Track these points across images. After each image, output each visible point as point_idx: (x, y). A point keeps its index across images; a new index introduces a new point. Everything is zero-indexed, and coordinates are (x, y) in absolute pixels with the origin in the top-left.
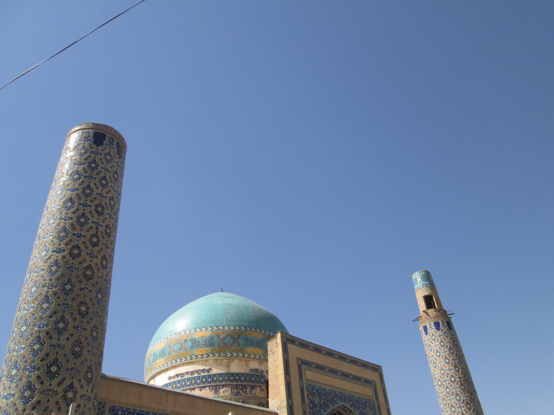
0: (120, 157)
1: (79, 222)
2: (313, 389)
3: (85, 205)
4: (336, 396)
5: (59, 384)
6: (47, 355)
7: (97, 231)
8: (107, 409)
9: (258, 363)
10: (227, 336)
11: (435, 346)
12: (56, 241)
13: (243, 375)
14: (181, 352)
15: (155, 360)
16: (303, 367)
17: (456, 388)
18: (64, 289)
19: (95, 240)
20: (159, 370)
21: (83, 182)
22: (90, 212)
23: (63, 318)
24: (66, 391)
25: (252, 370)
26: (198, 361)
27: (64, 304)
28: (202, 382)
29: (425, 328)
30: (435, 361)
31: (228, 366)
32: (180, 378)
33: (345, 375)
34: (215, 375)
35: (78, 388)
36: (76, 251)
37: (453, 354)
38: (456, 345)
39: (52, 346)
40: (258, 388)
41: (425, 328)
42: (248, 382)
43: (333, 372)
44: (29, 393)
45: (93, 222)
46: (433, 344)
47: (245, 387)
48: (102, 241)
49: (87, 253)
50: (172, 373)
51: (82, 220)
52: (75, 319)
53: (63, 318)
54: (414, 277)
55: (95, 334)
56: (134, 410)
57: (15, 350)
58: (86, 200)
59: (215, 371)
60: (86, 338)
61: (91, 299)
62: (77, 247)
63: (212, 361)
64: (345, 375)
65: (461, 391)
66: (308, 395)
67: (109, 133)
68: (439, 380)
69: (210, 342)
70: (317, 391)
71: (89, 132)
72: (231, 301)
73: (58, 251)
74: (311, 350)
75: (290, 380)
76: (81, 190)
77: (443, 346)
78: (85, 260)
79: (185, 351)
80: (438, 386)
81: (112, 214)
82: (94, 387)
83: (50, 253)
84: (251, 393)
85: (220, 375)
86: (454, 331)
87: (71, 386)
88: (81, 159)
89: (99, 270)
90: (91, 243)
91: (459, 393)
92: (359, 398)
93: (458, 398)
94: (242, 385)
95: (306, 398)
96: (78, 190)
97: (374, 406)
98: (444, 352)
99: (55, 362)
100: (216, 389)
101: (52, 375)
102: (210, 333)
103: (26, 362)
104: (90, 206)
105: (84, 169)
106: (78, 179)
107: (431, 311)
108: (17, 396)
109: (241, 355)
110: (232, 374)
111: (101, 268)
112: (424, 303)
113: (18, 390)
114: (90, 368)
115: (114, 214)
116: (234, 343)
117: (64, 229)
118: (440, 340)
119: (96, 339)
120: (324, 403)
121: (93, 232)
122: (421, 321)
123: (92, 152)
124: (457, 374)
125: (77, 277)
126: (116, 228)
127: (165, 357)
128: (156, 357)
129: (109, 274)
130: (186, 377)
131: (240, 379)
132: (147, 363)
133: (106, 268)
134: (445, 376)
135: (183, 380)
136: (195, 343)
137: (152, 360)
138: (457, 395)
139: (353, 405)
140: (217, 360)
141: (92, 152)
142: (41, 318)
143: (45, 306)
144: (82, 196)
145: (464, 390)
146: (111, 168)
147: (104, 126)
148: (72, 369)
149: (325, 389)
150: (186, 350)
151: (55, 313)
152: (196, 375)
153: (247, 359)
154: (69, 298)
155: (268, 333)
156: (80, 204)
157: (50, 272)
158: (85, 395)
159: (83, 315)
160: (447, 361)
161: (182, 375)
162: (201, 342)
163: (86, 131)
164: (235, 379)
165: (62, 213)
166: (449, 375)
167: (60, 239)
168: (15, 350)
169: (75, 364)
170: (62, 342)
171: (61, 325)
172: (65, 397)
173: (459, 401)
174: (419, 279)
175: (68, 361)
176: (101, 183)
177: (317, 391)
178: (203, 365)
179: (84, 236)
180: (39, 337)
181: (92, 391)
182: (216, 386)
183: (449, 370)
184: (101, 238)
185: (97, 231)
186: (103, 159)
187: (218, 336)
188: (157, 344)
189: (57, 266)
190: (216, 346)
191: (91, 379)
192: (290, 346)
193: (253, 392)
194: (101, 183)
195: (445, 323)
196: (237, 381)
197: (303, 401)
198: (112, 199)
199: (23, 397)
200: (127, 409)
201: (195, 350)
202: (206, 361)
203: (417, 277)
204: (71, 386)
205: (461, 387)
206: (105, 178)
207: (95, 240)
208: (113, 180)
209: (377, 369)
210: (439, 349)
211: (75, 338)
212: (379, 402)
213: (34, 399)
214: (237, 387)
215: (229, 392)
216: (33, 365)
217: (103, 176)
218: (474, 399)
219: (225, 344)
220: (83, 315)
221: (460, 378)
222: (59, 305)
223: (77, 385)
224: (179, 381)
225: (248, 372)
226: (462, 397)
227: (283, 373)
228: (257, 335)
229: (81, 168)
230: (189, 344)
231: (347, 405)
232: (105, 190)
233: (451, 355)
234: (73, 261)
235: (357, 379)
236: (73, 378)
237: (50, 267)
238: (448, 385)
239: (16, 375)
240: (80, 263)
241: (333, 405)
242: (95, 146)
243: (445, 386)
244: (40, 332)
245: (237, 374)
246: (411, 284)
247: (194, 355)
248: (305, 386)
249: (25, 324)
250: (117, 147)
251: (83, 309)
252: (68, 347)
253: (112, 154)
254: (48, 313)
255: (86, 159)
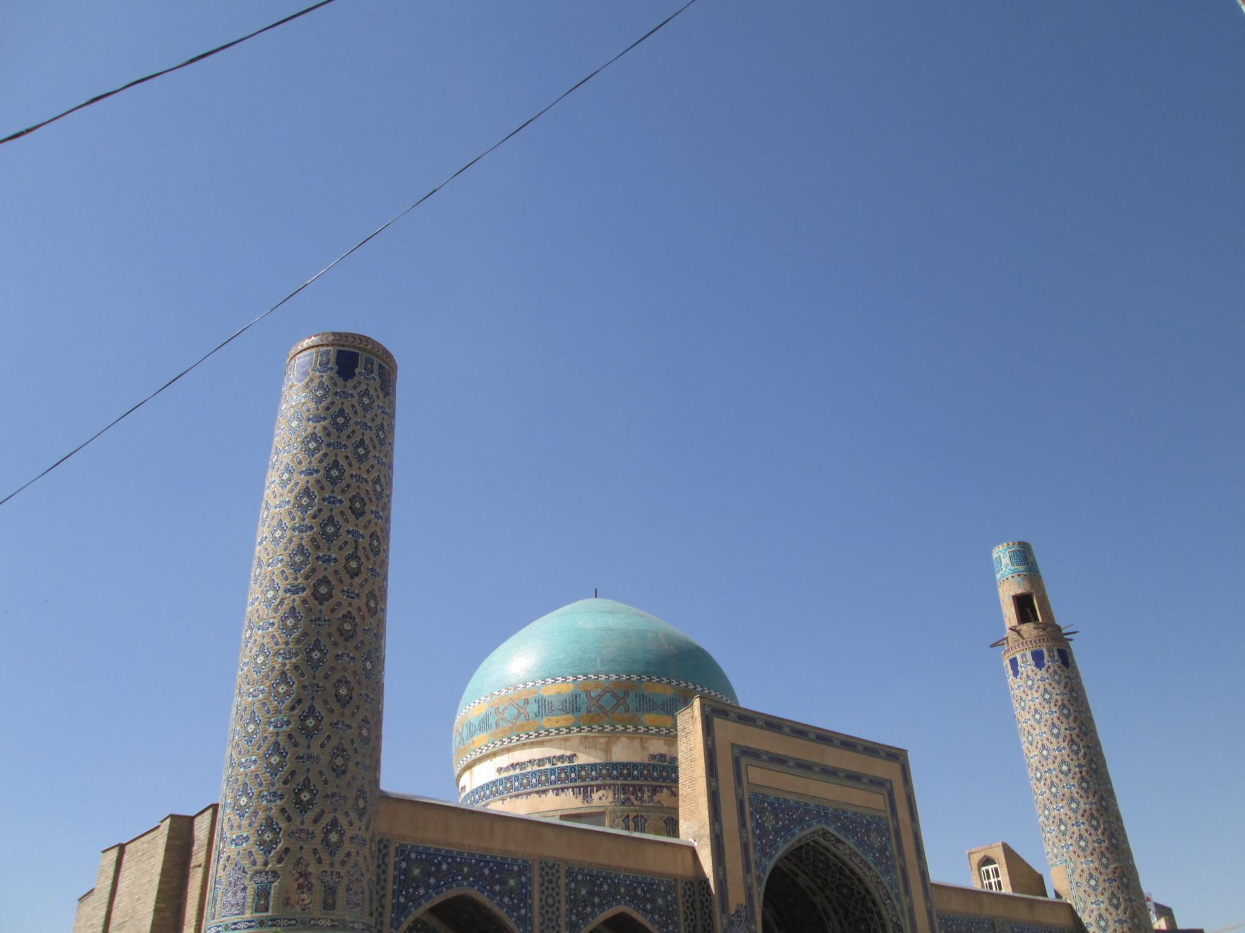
0: (387, 394)
1: (324, 533)
2: (762, 802)
3: (332, 501)
4: (808, 812)
5: (316, 821)
6: (293, 773)
7: (356, 548)
8: (392, 850)
9: (666, 744)
10: (605, 692)
11: (1033, 700)
12: (288, 571)
13: (635, 766)
14: (519, 722)
15: (471, 734)
16: (743, 761)
17: (1071, 786)
18: (310, 659)
19: (353, 564)
20: (478, 755)
21: (325, 455)
22: (342, 513)
23: (312, 709)
24: (327, 832)
25: (653, 757)
26: (551, 740)
27: (312, 685)
28: (559, 779)
29: (1014, 663)
30: (1032, 731)
31: (607, 750)
32: (518, 771)
33: (828, 772)
34: (582, 767)
35: (345, 826)
36: (323, 590)
37: (1067, 717)
38: (1076, 699)
39: (298, 758)
40: (665, 791)
41: (1014, 663)
42: (646, 779)
43: (804, 766)
44: (271, 836)
45: (348, 532)
46: (1029, 697)
47: (641, 788)
48: (368, 565)
49: (343, 591)
50: (504, 760)
51: (330, 529)
52: (331, 711)
53: (312, 709)
54: (995, 556)
55: (365, 732)
56: (436, 850)
57: (240, 764)
58: (333, 491)
59: (583, 759)
60: (352, 741)
61: (355, 673)
62: (325, 581)
63: (577, 741)
64: (828, 772)
65: (1082, 793)
66: (751, 814)
67: (365, 350)
68: (1037, 769)
69: (571, 705)
70: (771, 804)
71: (327, 353)
72: (611, 621)
73: (295, 590)
74: (762, 728)
75: (717, 788)
76: (322, 471)
77: (1048, 702)
78: (339, 604)
79: (524, 719)
80: (1034, 781)
81: (380, 510)
82: (369, 821)
83: (281, 593)
84: (652, 801)
85: (593, 766)
86: (1075, 668)
87: (334, 824)
88: (317, 409)
89: (364, 619)
90: (348, 572)
91: (1076, 795)
92: (855, 814)
93: (1074, 806)
94: (633, 786)
95: (748, 819)
96: (317, 471)
97: (888, 830)
98: (1050, 713)
99: (306, 785)
100: (585, 793)
101: (303, 807)
102: (571, 687)
103: (261, 785)
104: (341, 502)
105: (325, 428)
106: (317, 449)
107: (1027, 628)
108: (252, 840)
109: (631, 729)
110: (615, 766)
111: (367, 615)
112: (1013, 610)
113: (253, 831)
114: (361, 791)
115: (383, 509)
116: (618, 705)
117: (301, 549)
118: (1042, 689)
119: (367, 740)
120: (784, 826)
121: (349, 550)
122: (1006, 647)
123: (336, 394)
124: (1075, 757)
125: (330, 635)
126: (388, 533)
127: (489, 732)
128: (472, 730)
129: (381, 624)
130: (529, 769)
131: (629, 774)
132: (456, 740)
133: (375, 613)
134: (1050, 761)
135: (525, 775)
136: (544, 707)
137: (465, 735)
138: (1072, 799)
139: (844, 828)
140: (586, 737)
141: (336, 394)
142: (278, 711)
143: (282, 689)
144: (326, 484)
145: (1086, 791)
146: (373, 420)
147: (354, 336)
148: (333, 795)
149: (786, 801)
150: (527, 718)
151: (299, 701)
152: (548, 766)
153: (641, 735)
154: (320, 673)
155: (684, 684)
156: (323, 499)
157: (287, 631)
158: (357, 836)
159: (344, 702)
160: (1055, 731)
161: (521, 765)
162: (556, 704)
163: (322, 349)
164: (621, 774)
165: (293, 519)
166: (1058, 760)
167: (296, 567)
168: (240, 764)
169: (337, 786)
170: (315, 751)
171: (311, 722)
172: (326, 841)
173: (1075, 811)
174: (1006, 561)
175: (326, 782)
176: (356, 453)
177: (771, 804)
178: (561, 748)
179: (336, 560)
180: (276, 744)
181: (367, 829)
182: (586, 787)
183: (1059, 749)
184: (363, 560)
185: (356, 548)
186: (356, 404)
187: (587, 692)
188: (472, 707)
189: (295, 618)
190: (584, 712)
191: (365, 808)
192: (717, 722)
193: (656, 798)
194: (356, 453)
195: (1056, 653)
196: (625, 778)
197: (743, 824)
198: (377, 481)
199: (262, 843)
200: (425, 848)
201: (545, 719)
202: (566, 740)
203: (1002, 555)
204: (334, 824)
205: (1080, 785)
206: (362, 442)
207: (353, 564)
208: (377, 443)
209: (897, 756)
210: (1039, 708)
211: (334, 742)
212: (897, 821)
213: (280, 845)
214: (624, 788)
215: (610, 798)
216: (272, 790)
217: (358, 439)
218: (1106, 809)
219: (601, 707)
220: (344, 702)
221: (1080, 766)
222: (304, 687)
223: (343, 821)
224: (516, 776)
225: (646, 761)
226: (1082, 804)
227: (704, 774)
228: (661, 690)
229: (319, 426)
230: (533, 708)
231: (831, 829)
232: (365, 466)
233: (1064, 720)
234: (319, 607)
235: (854, 777)
236: (335, 810)
237: (284, 619)
238: (1055, 779)
239: (247, 806)
240: (332, 610)
241: (802, 829)
242: (340, 381)
243: (1048, 782)
244: (278, 734)
245: (625, 765)
246: (989, 568)
247: (542, 728)
248: (746, 797)
249: (253, 719)
250: (380, 375)
251: (343, 691)
252: (325, 759)
253: (372, 392)
254: (288, 702)
255: (328, 409)
